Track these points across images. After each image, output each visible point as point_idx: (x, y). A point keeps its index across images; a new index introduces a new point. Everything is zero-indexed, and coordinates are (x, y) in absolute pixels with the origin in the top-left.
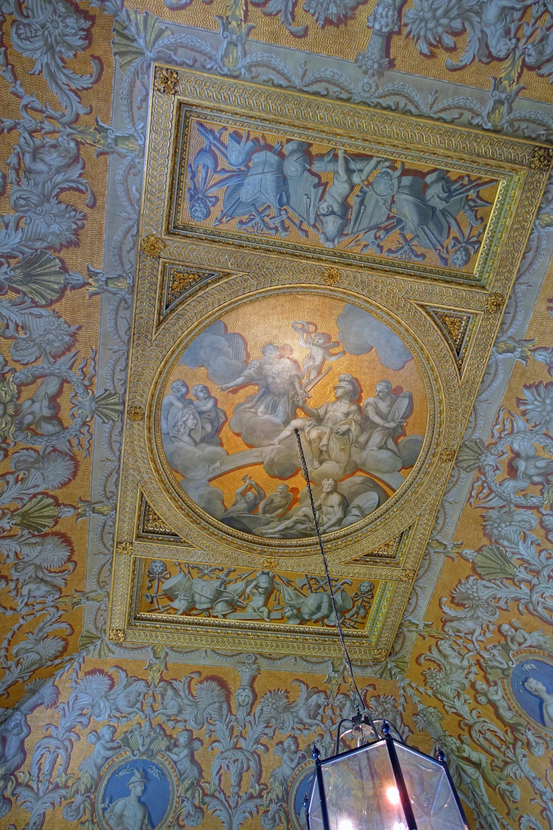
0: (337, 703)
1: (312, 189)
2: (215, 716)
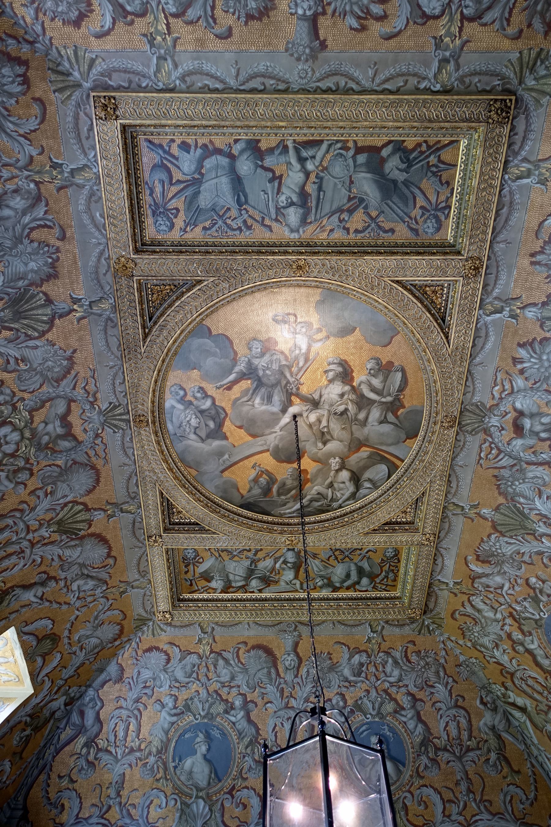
0: (379, 660)
1: (268, 184)
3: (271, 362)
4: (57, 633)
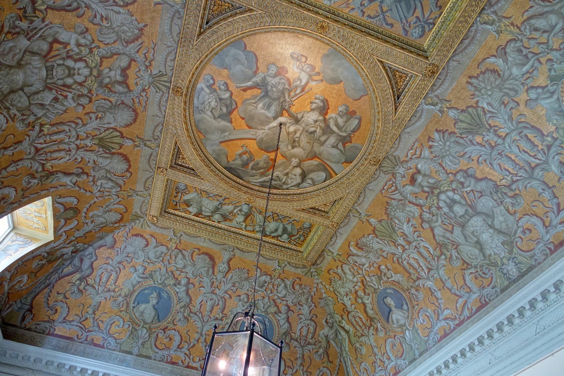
2: (204, 274)
3: (279, 83)
4: (79, 208)
